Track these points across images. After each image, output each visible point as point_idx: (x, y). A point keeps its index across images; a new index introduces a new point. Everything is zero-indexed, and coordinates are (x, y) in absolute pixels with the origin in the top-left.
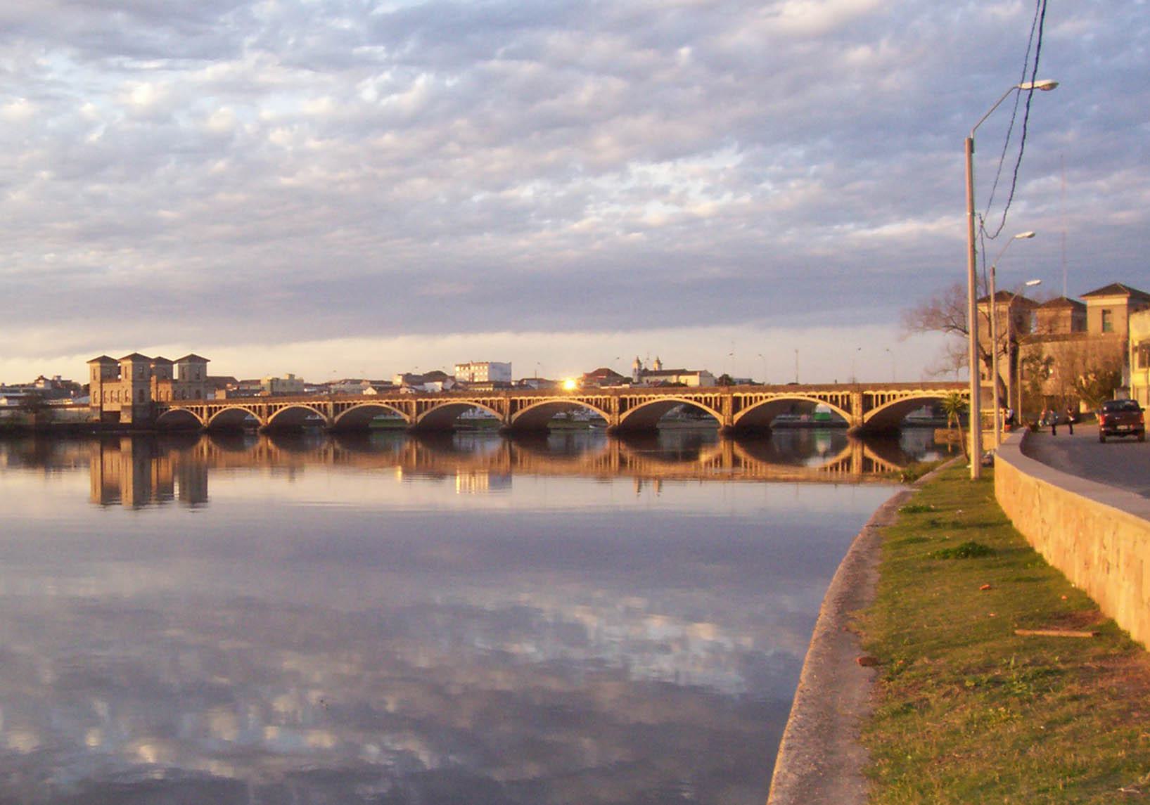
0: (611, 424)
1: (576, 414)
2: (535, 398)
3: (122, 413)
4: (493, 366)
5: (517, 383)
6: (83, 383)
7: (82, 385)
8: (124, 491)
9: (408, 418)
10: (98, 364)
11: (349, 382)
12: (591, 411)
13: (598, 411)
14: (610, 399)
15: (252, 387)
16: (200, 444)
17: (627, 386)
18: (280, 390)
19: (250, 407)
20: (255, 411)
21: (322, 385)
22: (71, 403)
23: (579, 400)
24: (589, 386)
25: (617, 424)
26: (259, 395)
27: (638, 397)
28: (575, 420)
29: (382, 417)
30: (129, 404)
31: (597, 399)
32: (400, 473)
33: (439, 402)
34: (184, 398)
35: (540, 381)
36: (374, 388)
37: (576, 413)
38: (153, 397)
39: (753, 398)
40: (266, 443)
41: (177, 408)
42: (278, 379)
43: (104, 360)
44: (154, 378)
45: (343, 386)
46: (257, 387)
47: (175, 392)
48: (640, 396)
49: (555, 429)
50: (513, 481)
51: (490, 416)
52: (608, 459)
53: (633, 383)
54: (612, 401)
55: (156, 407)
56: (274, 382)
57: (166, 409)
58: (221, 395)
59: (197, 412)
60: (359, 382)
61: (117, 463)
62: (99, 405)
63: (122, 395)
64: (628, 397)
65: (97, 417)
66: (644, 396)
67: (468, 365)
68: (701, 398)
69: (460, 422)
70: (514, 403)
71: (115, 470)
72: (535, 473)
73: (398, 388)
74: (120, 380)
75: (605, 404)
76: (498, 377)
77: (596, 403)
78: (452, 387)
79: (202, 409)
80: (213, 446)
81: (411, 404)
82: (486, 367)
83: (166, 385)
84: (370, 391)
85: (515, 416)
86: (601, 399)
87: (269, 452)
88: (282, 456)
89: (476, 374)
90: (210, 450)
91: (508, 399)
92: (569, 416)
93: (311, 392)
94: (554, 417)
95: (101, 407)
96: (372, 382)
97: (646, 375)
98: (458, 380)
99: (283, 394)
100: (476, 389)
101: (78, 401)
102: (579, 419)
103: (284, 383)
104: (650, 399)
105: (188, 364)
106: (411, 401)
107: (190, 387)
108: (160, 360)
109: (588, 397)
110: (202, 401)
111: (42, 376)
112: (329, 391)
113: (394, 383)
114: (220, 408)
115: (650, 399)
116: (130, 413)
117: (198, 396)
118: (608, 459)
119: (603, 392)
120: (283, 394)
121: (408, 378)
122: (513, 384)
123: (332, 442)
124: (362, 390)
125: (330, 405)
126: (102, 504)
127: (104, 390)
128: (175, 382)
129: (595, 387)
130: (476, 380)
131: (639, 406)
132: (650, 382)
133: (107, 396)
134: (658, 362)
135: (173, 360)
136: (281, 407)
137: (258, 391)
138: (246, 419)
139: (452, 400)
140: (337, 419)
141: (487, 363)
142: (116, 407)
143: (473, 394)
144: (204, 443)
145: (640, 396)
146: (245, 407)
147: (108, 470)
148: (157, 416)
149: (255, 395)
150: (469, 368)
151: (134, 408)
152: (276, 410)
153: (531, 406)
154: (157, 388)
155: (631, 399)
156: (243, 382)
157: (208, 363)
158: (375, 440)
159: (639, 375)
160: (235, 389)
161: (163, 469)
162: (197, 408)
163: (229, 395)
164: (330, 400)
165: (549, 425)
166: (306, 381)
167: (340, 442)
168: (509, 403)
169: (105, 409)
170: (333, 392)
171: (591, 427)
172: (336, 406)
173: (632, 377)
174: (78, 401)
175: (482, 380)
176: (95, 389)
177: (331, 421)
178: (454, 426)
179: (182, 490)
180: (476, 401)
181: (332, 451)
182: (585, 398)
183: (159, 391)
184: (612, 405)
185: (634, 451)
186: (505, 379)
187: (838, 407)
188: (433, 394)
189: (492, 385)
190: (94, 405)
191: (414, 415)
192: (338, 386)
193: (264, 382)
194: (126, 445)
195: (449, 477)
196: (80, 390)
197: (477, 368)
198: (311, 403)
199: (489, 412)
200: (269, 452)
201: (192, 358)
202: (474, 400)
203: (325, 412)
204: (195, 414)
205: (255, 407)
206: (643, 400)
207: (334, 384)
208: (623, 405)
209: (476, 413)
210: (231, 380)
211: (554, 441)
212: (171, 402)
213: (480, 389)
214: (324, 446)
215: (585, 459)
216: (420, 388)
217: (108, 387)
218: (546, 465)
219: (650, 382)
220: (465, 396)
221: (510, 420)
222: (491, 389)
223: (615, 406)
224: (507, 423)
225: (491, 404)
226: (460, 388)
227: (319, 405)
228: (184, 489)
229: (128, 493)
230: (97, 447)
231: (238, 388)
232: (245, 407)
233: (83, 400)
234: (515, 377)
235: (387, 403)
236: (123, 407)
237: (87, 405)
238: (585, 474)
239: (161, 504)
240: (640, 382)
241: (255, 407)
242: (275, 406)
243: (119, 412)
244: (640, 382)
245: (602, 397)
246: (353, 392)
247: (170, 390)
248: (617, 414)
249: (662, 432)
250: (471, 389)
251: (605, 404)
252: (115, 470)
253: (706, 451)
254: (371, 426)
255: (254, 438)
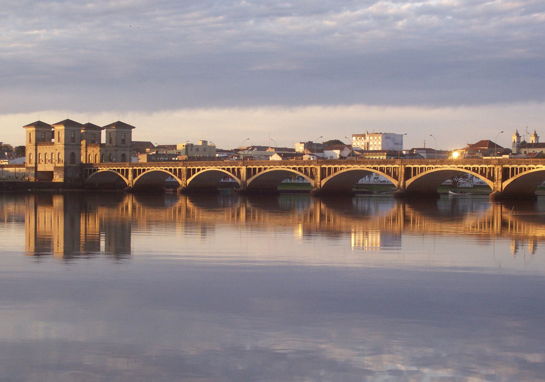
0: (494, 191)
1: (461, 181)
2: (427, 167)
3: (54, 173)
4: (387, 137)
5: (408, 153)
6: (15, 143)
7: (14, 147)
8: (55, 243)
9: (312, 183)
10: (33, 129)
11: (256, 149)
12: (474, 178)
13: (482, 178)
14: (493, 168)
15: (169, 152)
16: (126, 201)
17: (507, 156)
18: (196, 155)
19: (170, 170)
20: (175, 173)
21: (232, 151)
22: (7, 163)
23: (466, 168)
24: (472, 156)
25: (499, 190)
26: (177, 159)
27: (519, 167)
28: (460, 186)
29: (288, 181)
30: (62, 165)
31: (482, 168)
32: (300, 231)
33: (341, 168)
34: (110, 161)
35: (429, 151)
36: (280, 155)
37: (461, 180)
38: (83, 159)
39: (427, 168)
40: (184, 202)
41: (105, 169)
42: (192, 144)
43: (39, 125)
44: (83, 143)
45: (250, 153)
46: (174, 152)
47: (103, 155)
48: (521, 166)
49: (443, 194)
50: (402, 239)
51: (384, 181)
52: (491, 222)
53: (513, 154)
54: (496, 170)
55: (88, 168)
56: (189, 147)
57: (95, 170)
58: (143, 158)
59: (123, 174)
60: (265, 148)
61: (50, 221)
62: (34, 165)
63: (55, 157)
64: (510, 167)
65: (32, 179)
66: (525, 166)
67: (364, 136)
68: (470, 168)
69: (358, 186)
70: (408, 170)
71: (48, 225)
72: (423, 233)
73: (301, 155)
74: (53, 143)
75: (490, 173)
76: (391, 147)
77: (482, 171)
78: (349, 155)
79: (127, 170)
80: (137, 203)
81: (316, 169)
82: (380, 138)
83: (95, 149)
84: (276, 157)
85: (409, 182)
86: (486, 168)
87: (188, 211)
88: (202, 215)
89: (371, 143)
90: (134, 208)
91: (403, 166)
92: (454, 182)
93: (223, 157)
94: (443, 184)
95: (36, 167)
96: (277, 149)
97: (524, 147)
98: (354, 149)
99: (199, 159)
100: (378, 158)
101: (12, 162)
102: (463, 186)
103: (198, 148)
104: (530, 169)
105: (115, 130)
106: (316, 167)
107: (116, 150)
108: (89, 126)
109: (474, 166)
110: (128, 164)
111: (353, 135)
112: (239, 157)
113: (297, 150)
114: (144, 170)
115: (530, 169)
116: (62, 173)
117: (124, 159)
118: (491, 222)
119: (487, 162)
120: (199, 159)
121: (309, 146)
122: (404, 152)
123: (244, 201)
124: (268, 156)
125: (243, 170)
126: (35, 255)
127: (38, 153)
128: (102, 146)
129: (477, 157)
130: (371, 149)
131: (519, 175)
132: (527, 153)
133: (42, 157)
134: (536, 135)
135: (101, 126)
136: (199, 170)
137: (176, 156)
138: (166, 180)
139: (352, 166)
140: (249, 182)
141: (381, 133)
142: (49, 168)
143: (372, 162)
144: (129, 201)
145: (521, 166)
146: (166, 169)
147: (41, 226)
148: (86, 177)
149: (174, 159)
150: (365, 139)
151: (66, 169)
152: (194, 173)
153: (424, 173)
154: (86, 151)
155: (513, 169)
156: (160, 147)
157: (133, 130)
158: (282, 201)
159: (518, 146)
160: (155, 153)
161: (91, 226)
162: (123, 170)
163: (150, 158)
164: (243, 165)
165: (439, 191)
166: (219, 147)
167: (251, 202)
168: (403, 171)
169: (40, 168)
170: (242, 157)
171: (450, 192)
172: (248, 170)
173: (511, 148)
174: (12, 162)
175: (376, 149)
176: (30, 151)
177: (244, 183)
178: (354, 190)
179: (108, 244)
180: (374, 168)
181: (244, 211)
182: (472, 167)
183: (88, 154)
184: (496, 174)
185: (193, 204)
186: (396, 148)
187: (230, 172)
188: (332, 161)
189: (386, 154)
190: (29, 165)
191: (319, 179)
192: (246, 152)
193: (180, 147)
194: (58, 202)
195: (344, 236)
196: (12, 151)
197: (371, 138)
198: (226, 167)
199: (384, 177)
200: (188, 211)
201: (119, 125)
202: (372, 167)
203: (239, 176)
204: (121, 176)
205: (175, 170)
206: (431, 168)
207: (243, 150)
208: (506, 174)
209: (372, 179)
210: (149, 145)
211: (443, 205)
212: (98, 164)
213: (374, 157)
214: (238, 205)
215: (469, 221)
216: (320, 155)
217: (42, 149)
218: (437, 226)
219: (527, 153)
220: (364, 163)
221: (404, 183)
222: (385, 157)
223: (498, 175)
224: (402, 187)
225: (388, 171)
226: (358, 156)
227: (233, 169)
228: (109, 243)
229: (59, 246)
230: (32, 202)
231: (157, 152)
232: (166, 169)
233: (19, 161)
234: (407, 146)
235: (294, 168)
236: (56, 168)
237: (23, 166)
238: (468, 234)
239: (118, 258)
240: (518, 153)
241: (175, 170)
242: (194, 170)
243: (52, 172)
244: (518, 153)
245: (487, 167)
246: (259, 158)
247: (99, 153)
248: (500, 181)
249: (539, 199)
250: (367, 157)
251: (490, 173)
252: (48, 225)
253: (55, 198)
254: (280, 188)
255: (174, 198)
